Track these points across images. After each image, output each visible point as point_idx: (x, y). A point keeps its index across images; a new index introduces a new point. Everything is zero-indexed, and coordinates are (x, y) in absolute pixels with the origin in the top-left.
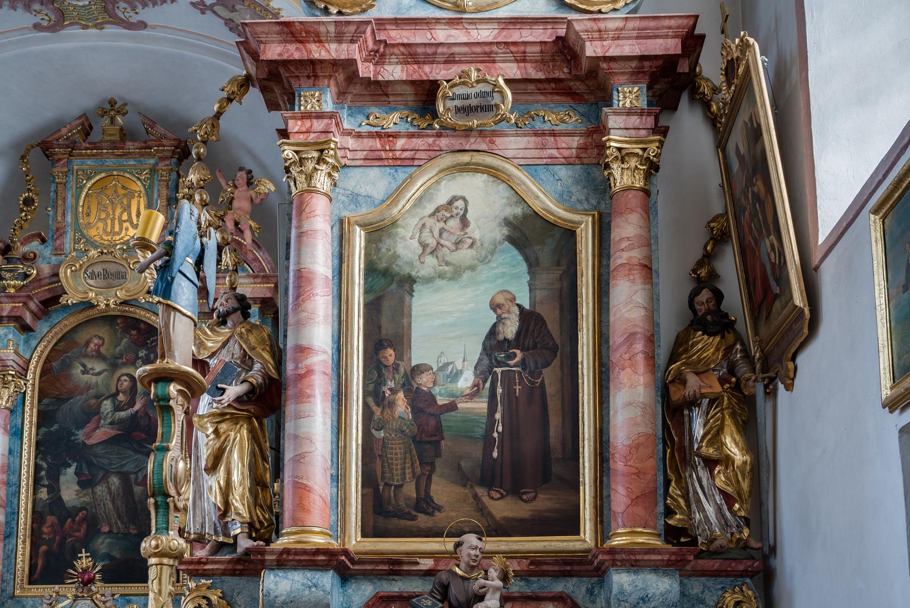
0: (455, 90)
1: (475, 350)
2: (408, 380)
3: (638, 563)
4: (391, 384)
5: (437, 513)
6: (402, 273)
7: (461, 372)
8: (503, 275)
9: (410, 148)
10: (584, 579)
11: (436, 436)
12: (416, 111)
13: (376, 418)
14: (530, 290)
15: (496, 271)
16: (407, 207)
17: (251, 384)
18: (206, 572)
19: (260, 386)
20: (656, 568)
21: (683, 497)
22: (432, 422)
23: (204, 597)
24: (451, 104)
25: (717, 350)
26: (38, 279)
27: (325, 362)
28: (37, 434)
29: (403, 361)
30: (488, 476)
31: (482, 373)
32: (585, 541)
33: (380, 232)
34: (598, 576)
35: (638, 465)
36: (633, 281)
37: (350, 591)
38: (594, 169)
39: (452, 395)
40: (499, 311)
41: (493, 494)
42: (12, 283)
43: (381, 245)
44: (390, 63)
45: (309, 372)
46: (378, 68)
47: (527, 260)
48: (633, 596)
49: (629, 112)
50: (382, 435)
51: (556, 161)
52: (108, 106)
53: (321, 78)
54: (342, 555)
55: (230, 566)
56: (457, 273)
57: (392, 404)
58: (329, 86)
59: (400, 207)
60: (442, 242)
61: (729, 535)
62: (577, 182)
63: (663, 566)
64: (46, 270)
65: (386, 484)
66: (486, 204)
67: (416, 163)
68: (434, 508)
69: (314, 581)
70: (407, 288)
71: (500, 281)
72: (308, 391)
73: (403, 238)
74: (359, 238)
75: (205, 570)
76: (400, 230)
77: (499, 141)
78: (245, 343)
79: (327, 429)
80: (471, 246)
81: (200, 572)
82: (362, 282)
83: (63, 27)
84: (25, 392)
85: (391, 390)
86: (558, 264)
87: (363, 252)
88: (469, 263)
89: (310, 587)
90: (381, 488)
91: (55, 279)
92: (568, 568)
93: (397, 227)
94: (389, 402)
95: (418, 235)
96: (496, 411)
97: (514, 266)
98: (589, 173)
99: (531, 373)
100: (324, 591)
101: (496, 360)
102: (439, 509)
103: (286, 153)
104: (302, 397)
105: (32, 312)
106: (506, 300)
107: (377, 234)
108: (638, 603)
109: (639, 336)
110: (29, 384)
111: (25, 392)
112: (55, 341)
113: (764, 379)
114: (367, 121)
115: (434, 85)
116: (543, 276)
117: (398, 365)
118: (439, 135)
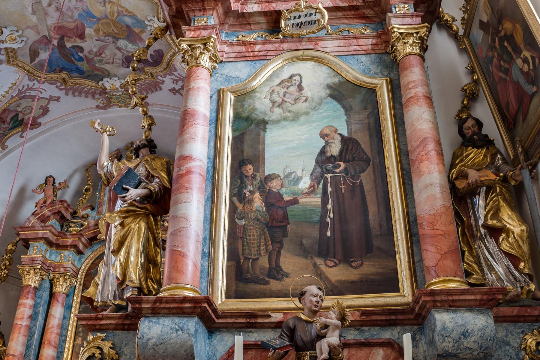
0: (291, 14)
1: (311, 164)
2: (262, 185)
3: (456, 304)
4: (250, 188)
5: (285, 279)
6: (258, 118)
7: (301, 178)
8: (328, 117)
9: (264, 50)
10: (407, 327)
11: (283, 222)
12: (268, 32)
13: (239, 211)
14: (347, 125)
15: (323, 114)
16: (262, 81)
17: (150, 189)
18: (102, 327)
19: (156, 193)
20: (471, 307)
21: (476, 263)
22: (281, 212)
23: (98, 348)
24: (288, 22)
25: (485, 156)
26: (88, 227)
27: (201, 167)
28: (80, 308)
29: (259, 172)
30: (324, 250)
31: (316, 178)
32: (404, 296)
33: (244, 96)
34: (419, 324)
35: (443, 229)
36: (421, 106)
37: (215, 341)
38: (384, 56)
39: (295, 193)
40: (326, 138)
41: (329, 263)
42: (75, 229)
43: (244, 103)
44: (251, 3)
45: (189, 172)
46: (244, 6)
47: (344, 107)
48: (455, 332)
49: (404, 16)
50: (243, 223)
51: (359, 53)
52: (130, 145)
53: (208, 10)
54: (204, 303)
55: (120, 322)
56: (296, 117)
57: (250, 202)
58: (212, 15)
59: (257, 81)
60: (285, 99)
61: (519, 289)
62: (373, 63)
63: (476, 306)
64: (92, 222)
65: (246, 258)
66: (314, 78)
67: (268, 58)
68: (282, 275)
69: (181, 325)
70: (262, 127)
71: (326, 120)
72: (187, 185)
73: (260, 99)
74: (230, 100)
75: (101, 325)
76: (258, 94)
77: (321, 43)
78: (149, 166)
79: (200, 213)
80: (305, 101)
81: (97, 327)
82: (231, 124)
83: (110, 107)
84: (75, 286)
85: (250, 191)
86: (365, 109)
87: (232, 107)
88: (304, 110)
89: (177, 331)
90: (242, 261)
91: (96, 227)
92: (393, 317)
93: (255, 92)
94: (249, 200)
95: (269, 96)
96: (327, 203)
97: (335, 111)
98: (381, 58)
99: (352, 177)
100: (188, 333)
101: (326, 169)
102: (287, 275)
103: (182, 45)
104: (184, 189)
105: (83, 243)
106: (331, 131)
107: (242, 97)
108: (460, 338)
109: (430, 140)
110: (78, 281)
111: (75, 286)
112: (94, 259)
113: (528, 166)
114: (237, 39)
115: (279, 13)
116: (356, 116)
117: (255, 175)
118: (282, 42)
